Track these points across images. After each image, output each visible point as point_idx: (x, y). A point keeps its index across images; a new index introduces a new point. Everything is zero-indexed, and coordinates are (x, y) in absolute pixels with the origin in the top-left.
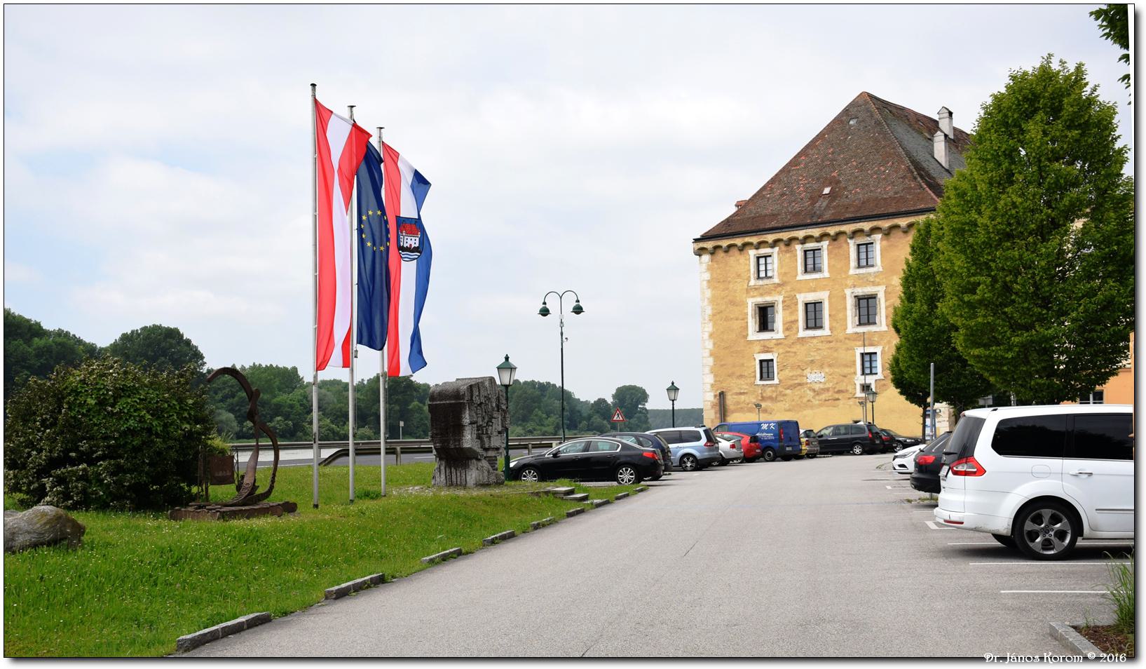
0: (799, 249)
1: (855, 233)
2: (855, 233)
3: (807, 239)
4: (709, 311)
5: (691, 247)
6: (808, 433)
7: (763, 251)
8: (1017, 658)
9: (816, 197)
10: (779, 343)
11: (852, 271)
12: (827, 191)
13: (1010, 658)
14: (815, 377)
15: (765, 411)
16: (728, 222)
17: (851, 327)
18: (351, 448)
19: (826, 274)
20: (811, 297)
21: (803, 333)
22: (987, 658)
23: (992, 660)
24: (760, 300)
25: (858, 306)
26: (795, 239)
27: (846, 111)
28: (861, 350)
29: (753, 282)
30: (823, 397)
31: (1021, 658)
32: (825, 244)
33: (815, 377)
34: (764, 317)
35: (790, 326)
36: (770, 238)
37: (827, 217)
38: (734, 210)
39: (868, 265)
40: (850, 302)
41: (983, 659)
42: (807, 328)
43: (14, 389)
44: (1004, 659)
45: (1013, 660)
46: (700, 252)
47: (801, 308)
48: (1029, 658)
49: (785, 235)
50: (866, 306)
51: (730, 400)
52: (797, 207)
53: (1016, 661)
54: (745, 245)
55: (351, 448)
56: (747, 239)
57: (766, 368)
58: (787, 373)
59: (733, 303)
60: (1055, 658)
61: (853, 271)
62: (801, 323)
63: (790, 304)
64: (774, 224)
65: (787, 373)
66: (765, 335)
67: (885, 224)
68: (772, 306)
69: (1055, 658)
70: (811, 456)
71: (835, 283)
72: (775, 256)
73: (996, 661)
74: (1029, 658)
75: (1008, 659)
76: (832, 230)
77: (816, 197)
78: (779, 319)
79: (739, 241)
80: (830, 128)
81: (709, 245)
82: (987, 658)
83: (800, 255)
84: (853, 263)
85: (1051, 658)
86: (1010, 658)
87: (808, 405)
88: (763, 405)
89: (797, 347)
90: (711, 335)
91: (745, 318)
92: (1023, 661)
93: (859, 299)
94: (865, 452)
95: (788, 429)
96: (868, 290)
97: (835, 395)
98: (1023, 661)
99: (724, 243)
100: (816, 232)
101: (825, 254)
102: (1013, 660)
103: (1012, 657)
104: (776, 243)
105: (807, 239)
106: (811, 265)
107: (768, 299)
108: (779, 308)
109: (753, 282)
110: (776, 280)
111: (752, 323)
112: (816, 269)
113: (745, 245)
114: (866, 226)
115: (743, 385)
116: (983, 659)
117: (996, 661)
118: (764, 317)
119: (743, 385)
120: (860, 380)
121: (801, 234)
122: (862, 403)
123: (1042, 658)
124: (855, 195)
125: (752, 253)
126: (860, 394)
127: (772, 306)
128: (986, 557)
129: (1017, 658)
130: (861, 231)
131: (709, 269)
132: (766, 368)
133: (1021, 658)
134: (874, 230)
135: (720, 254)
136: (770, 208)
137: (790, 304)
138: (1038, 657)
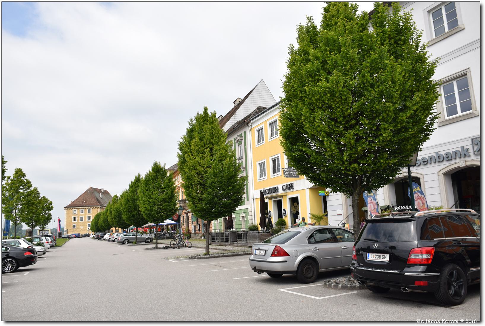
0: (80, 210)
1: (88, 208)
2: (88, 208)
3: (81, 208)
4: (66, 218)
5: (64, 208)
6: (81, 235)
7: (75, 210)
8: (431, 321)
9: (83, 202)
10: (76, 222)
11: (88, 213)
12: (84, 202)
13: (427, 321)
14: (82, 227)
15: (74, 232)
16: (69, 205)
17: (87, 220)
18: (5, 238)
19: (84, 213)
20: (82, 216)
21: (80, 221)
22: (418, 322)
23: (420, 322)
24: (74, 216)
25: (88, 218)
26: (73, 209)
27: (88, 190)
28: (88, 224)
29: (73, 214)
30: (83, 230)
31: (432, 321)
32: (84, 209)
33: (82, 227)
34: (75, 219)
35: (78, 220)
36: (76, 208)
37: (84, 205)
38: (71, 203)
39: (90, 212)
40: (87, 217)
41: (416, 322)
42: (81, 220)
43: (199, 192)
44: (425, 322)
45: (429, 322)
46: (65, 209)
47: (80, 218)
48: (435, 322)
49: (78, 208)
50: (89, 218)
51: (68, 230)
52: (80, 204)
53: (430, 323)
54: (72, 209)
55: (5, 238)
56: (79, 208)
57: (74, 226)
58: (78, 226)
59: (70, 217)
60: (447, 322)
61: (88, 213)
62: (80, 220)
63: (78, 217)
64: (77, 206)
65: (78, 226)
66: (75, 221)
67: (92, 207)
68: (76, 217)
69: (447, 322)
70: (81, 237)
71: (85, 215)
72: (77, 211)
73: (421, 323)
74: (435, 322)
75: (427, 322)
76: (85, 207)
77: (83, 202)
78: (77, 219)
79: (71, 208)
80: (85, 192)
81: (67, 208)
82: (418, 322)
83: (88, 210)
84: (88, 212)
85: (445, 321)
86: (427, 321)
87: (80, 231)
88: (74, 231)
89: (79, 223)
90: (66, 221)
91: (72, 219)
92: (433, 323)
93: (88, 217)
94: (88, 237)
95: (79, 234)
96: (90, 216)
97: (84, 230)
98: (433, 323)
99: (69, 208)
100: (83, 208)
101: (84, 210)
102: (429, 322)
103: (428, 321)
104: (77, 209)
105: (81, 208)
106: (82, 212)
107: (75, 216)
108: (77, 218)
109: (73, 214)
110: (77, 214)
111: (73, 220)
112: (82, 212)
113: (72, 209)
114: (90, 207)
115: (71, 228)
116: (416, 322)
117: (421, 323)
118: (75, 219)
119: (71, 228)
120: (88, 228)
121: (81, 208)
122: (88, 231)
123: (441, 322)
124: (88, 203)
125: (73, 210)
126: (88, 229)
127: (76, 217)
128: (325, 272)
129: (431, 321)
130: (89, 208)
131: (66, 212)
132: (74, 226)
133: (432, 321)
134: (91, 208)
135: (68, 210)
136: (76, 203)
137: (78, 217)
138: (439, 321)
